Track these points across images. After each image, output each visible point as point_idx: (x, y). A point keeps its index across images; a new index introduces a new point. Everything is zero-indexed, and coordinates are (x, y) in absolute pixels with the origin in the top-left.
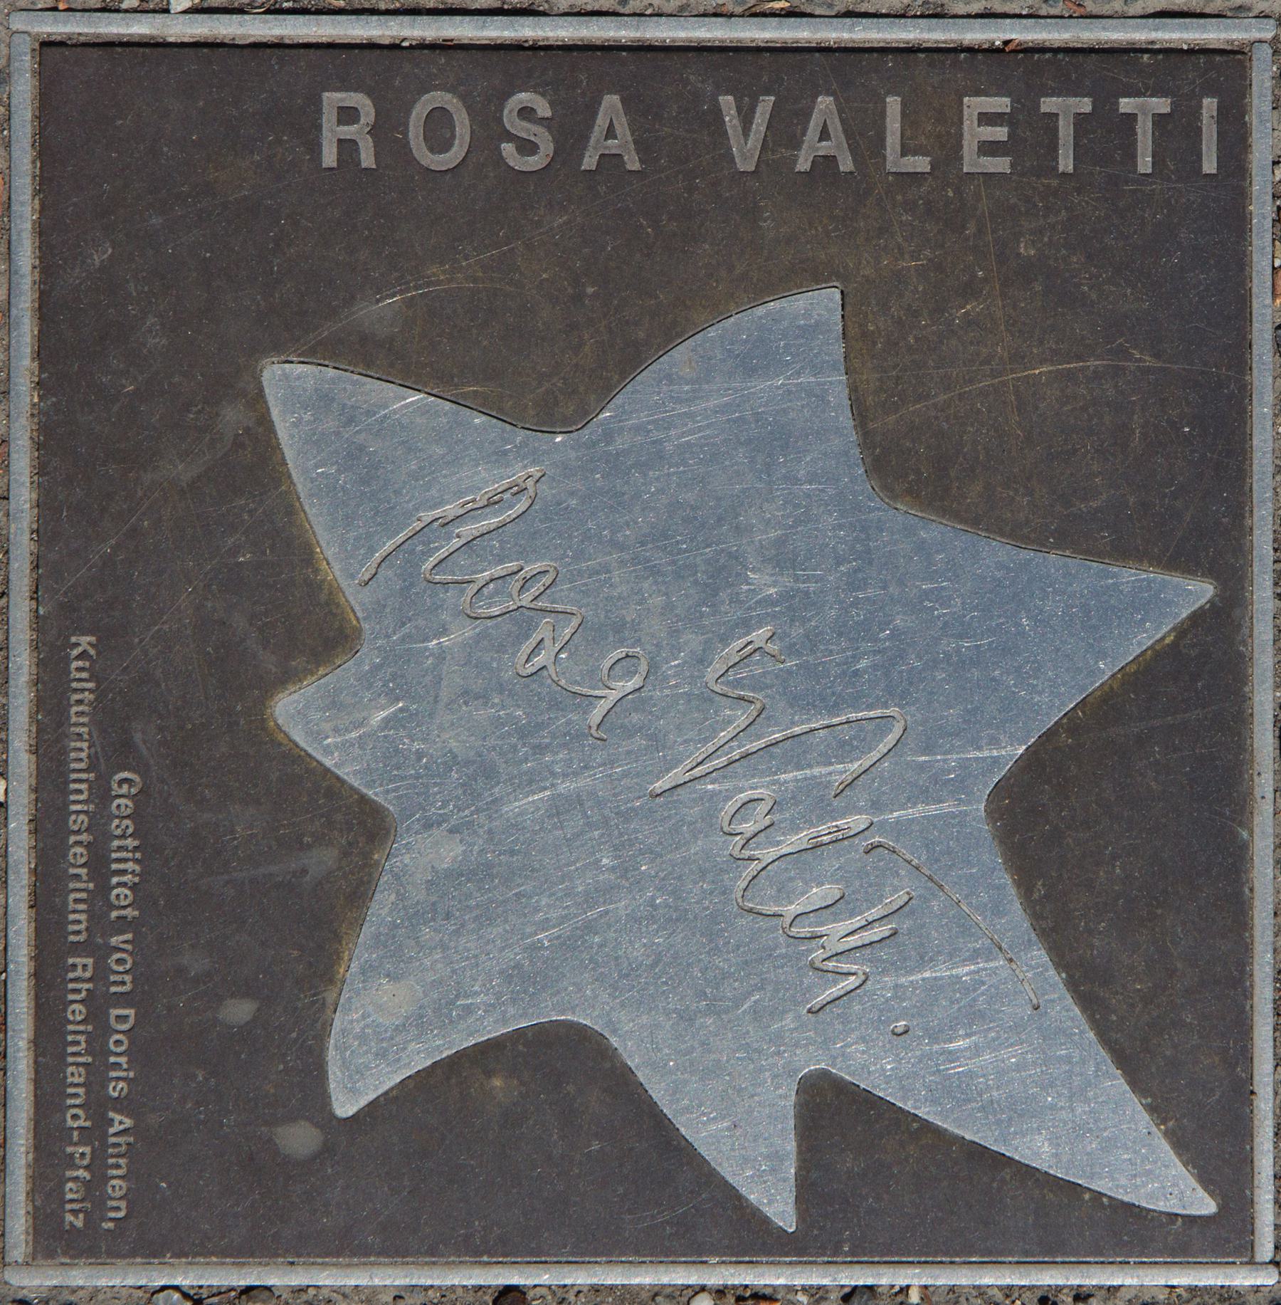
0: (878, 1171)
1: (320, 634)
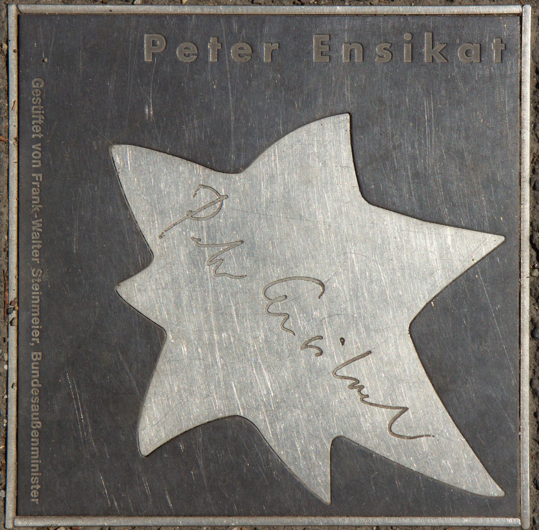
0: (364, 476)
1: (139, 257)
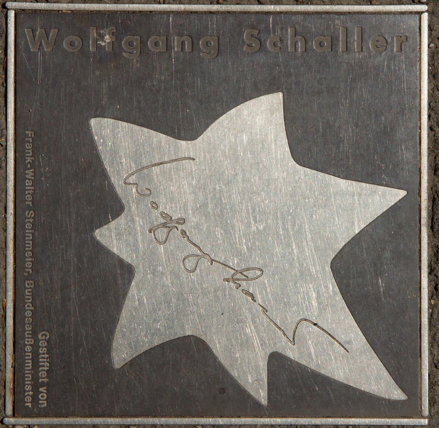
0: (294, 384)
